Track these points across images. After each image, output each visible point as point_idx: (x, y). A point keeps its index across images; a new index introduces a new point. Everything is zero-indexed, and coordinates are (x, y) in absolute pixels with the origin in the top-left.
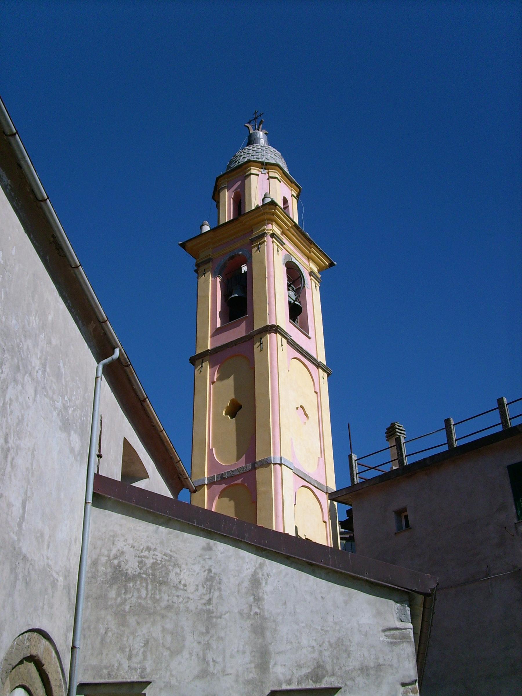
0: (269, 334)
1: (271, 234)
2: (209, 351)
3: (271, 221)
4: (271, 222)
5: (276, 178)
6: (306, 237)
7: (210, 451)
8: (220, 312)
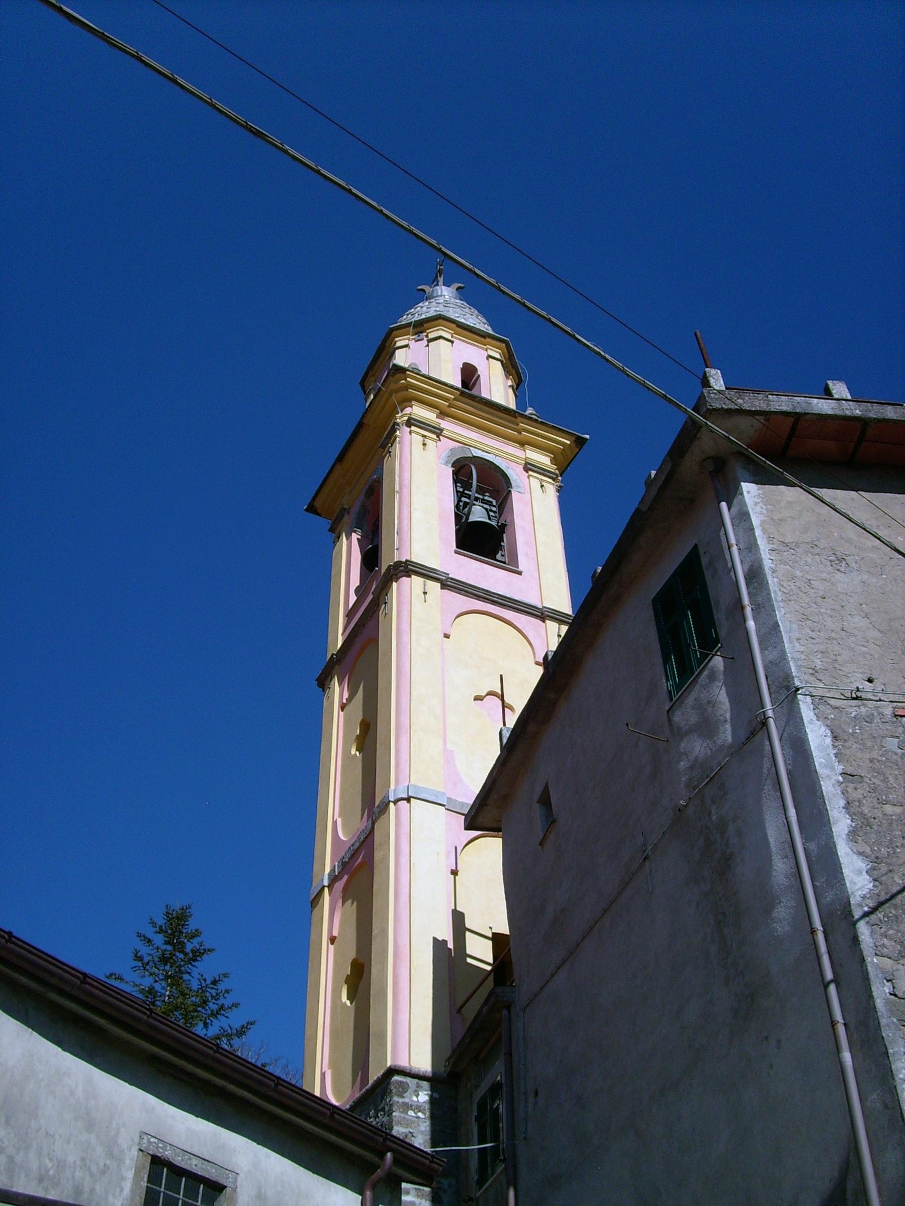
0: (396, 582)
1: (407, 421)
2: (335, 656)
3: (407, 401)
4: (408, 404)
5: (440, 337)
6: (500, 409)
7: (335, 823)
8: (358, 587)
